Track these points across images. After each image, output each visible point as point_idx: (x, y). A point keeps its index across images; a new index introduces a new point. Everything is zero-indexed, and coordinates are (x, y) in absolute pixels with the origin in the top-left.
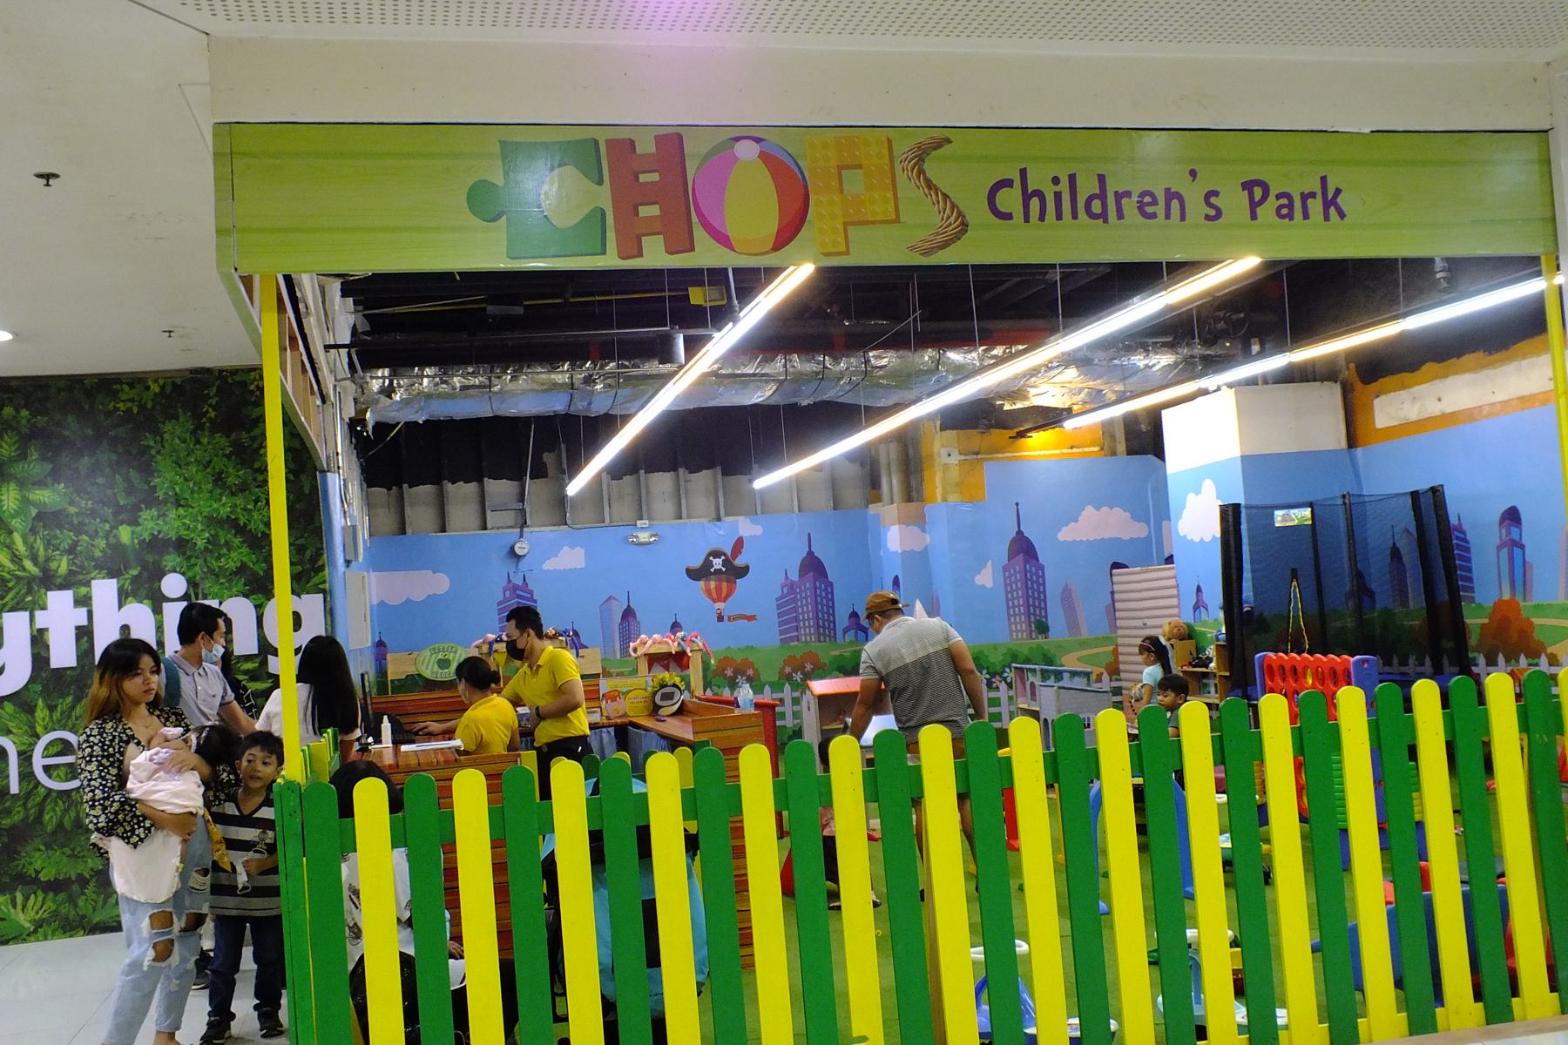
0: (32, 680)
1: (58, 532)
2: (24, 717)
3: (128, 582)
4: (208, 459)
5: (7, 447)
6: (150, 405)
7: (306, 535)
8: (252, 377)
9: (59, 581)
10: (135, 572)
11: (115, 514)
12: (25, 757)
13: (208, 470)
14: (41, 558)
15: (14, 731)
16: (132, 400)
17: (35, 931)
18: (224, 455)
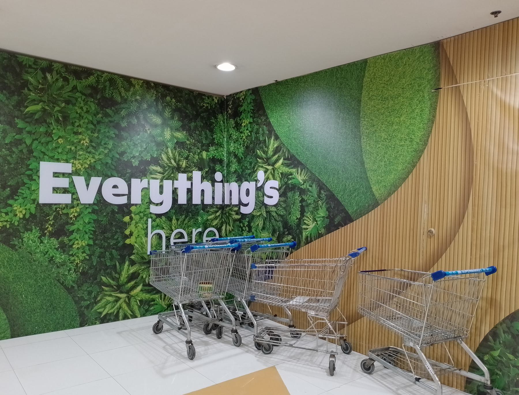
0: (172, 208)
1: (183, 150)
2: (168, 222)
3: (205, 173)
4: (46, 250)
5: (167, 112)
6: (16, 224)
7: (93, 286)
8: (72, 211)
9: (182, 170)
10: (207, 170)
11: (202, 146)
12: (168, 239)
13: (46, 256)
14: (177, 160)
15: (165, 228)
16: (7, 221)
17: (167, 309)
18: (55, 248)
